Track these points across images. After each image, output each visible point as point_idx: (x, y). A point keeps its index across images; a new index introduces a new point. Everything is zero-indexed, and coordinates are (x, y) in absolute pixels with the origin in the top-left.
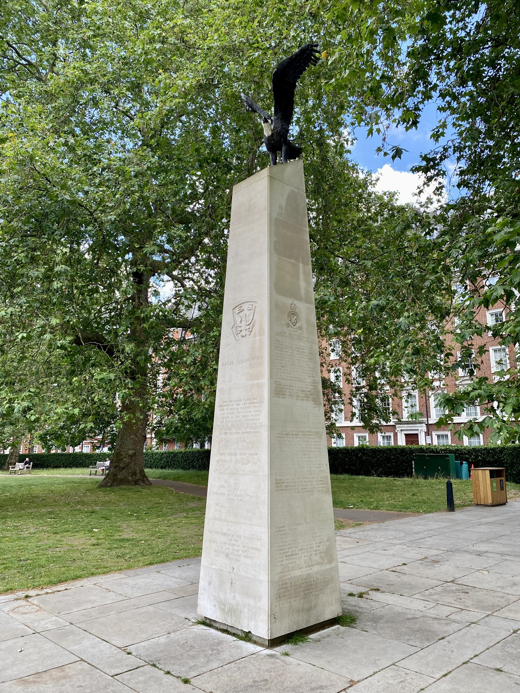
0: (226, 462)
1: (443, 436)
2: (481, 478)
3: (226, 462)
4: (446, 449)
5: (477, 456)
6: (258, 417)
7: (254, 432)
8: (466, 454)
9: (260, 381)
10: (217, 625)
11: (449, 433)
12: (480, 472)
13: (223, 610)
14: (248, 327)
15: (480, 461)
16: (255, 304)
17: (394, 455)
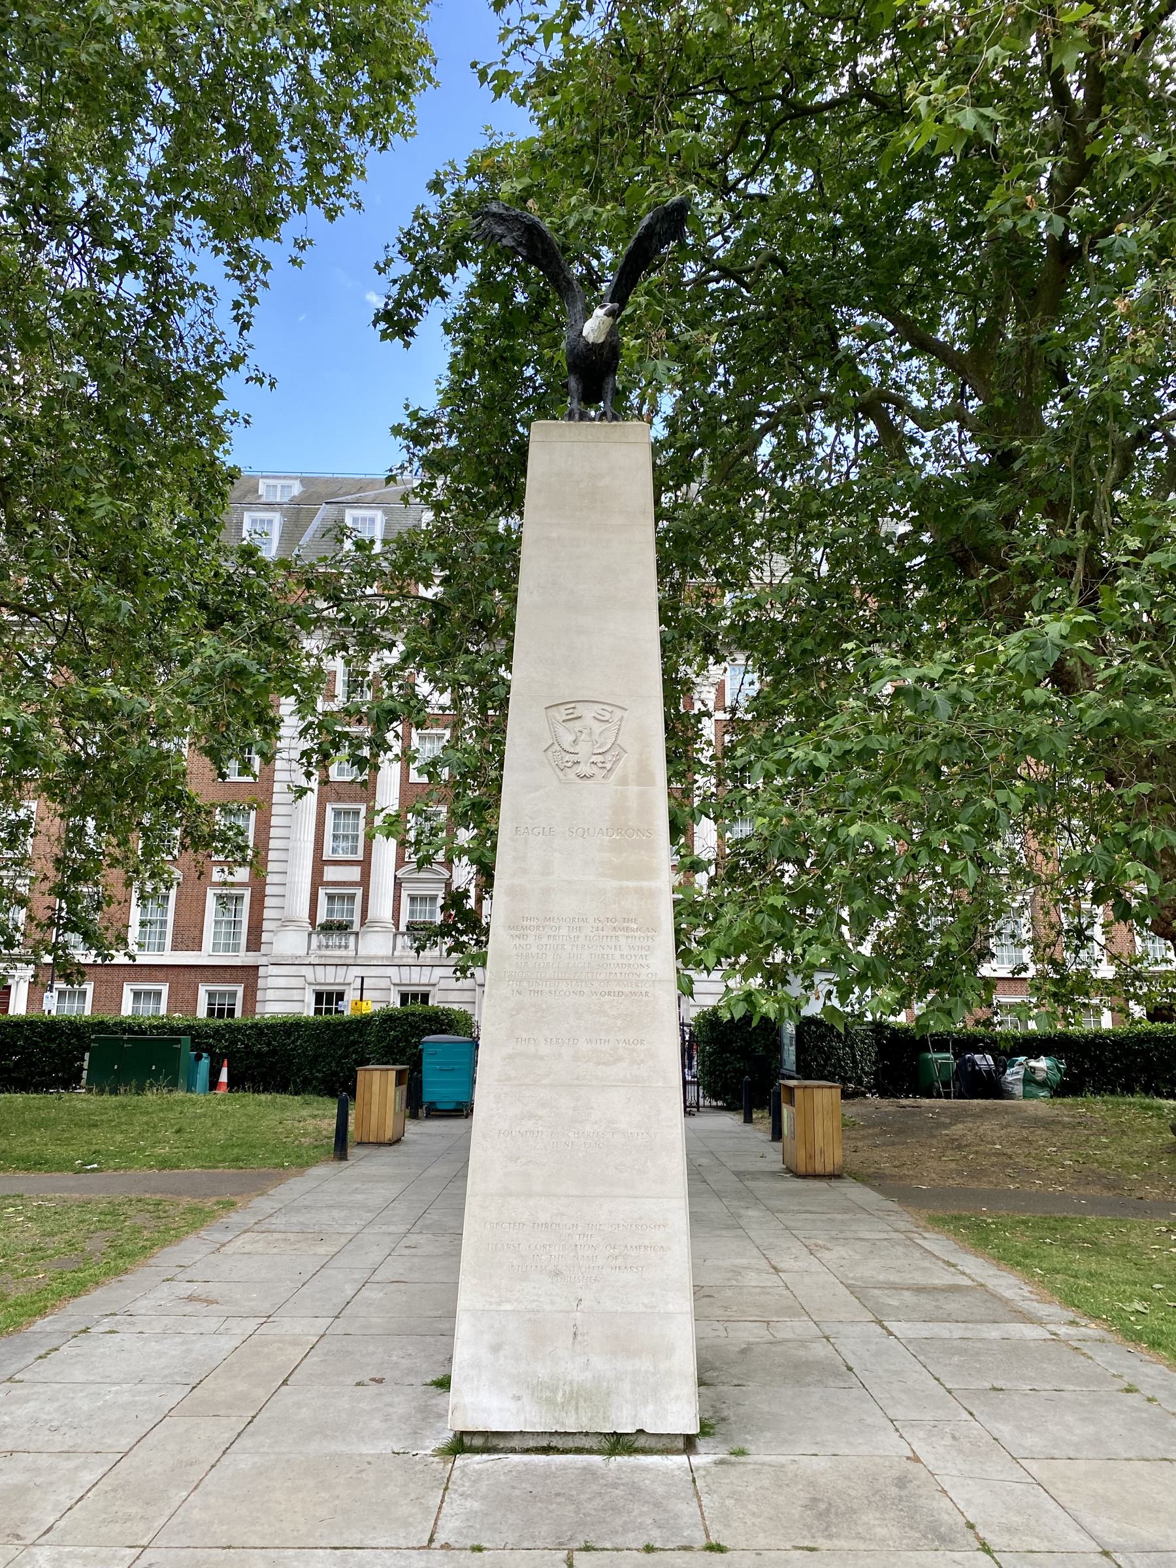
0: (542, 1058)
1: (148, 993)
2: (376, 1088)
3: (542, 1058)
5: (234, 1042)
6: (644, 962)
7: (633, 994)
9: (645, 884)
10: (515, 1443)
11: (165, 989)
12: (377, 1074)
13: (550, 1402)
14: (599, 758)
15: (238, 1051)
16: (619, 713)
17: (27, 1038)
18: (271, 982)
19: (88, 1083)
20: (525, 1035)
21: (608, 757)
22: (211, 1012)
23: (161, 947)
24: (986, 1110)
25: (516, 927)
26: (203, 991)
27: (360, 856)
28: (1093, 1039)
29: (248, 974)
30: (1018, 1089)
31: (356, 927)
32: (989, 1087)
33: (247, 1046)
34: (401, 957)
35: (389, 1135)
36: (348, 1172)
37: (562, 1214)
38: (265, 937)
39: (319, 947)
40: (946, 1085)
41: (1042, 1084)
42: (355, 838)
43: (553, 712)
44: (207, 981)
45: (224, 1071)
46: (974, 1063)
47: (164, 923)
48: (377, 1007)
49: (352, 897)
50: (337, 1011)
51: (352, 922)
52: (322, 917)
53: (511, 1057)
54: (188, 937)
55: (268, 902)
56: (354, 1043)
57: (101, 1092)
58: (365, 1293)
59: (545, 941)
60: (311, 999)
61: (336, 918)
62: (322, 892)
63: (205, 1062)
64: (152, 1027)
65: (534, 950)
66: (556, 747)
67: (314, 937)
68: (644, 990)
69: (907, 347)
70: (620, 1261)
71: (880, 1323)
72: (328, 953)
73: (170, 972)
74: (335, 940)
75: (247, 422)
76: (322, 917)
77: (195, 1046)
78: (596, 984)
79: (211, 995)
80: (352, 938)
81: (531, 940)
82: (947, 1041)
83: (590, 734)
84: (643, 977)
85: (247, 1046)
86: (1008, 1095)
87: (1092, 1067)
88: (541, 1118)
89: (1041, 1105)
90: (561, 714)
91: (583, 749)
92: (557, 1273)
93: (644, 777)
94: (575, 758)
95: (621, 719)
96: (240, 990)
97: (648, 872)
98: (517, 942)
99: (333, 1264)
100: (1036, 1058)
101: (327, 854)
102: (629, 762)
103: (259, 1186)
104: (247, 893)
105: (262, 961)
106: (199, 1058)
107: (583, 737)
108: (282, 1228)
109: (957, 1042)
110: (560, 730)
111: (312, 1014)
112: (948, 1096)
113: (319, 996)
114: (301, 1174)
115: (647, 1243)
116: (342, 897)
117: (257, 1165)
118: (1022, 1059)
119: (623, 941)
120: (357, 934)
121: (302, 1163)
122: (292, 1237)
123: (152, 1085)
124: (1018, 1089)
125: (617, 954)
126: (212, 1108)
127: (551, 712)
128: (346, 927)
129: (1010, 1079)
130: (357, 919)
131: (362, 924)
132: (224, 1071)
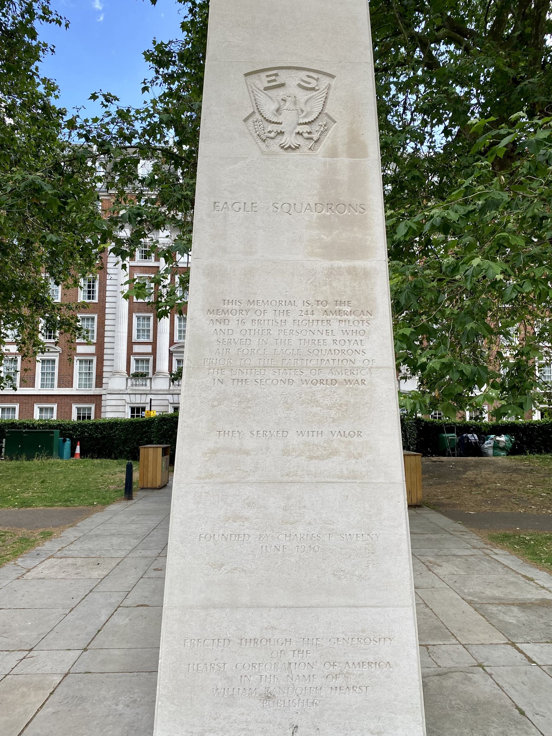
0: (247, 453)
1: (47, 409)
2: (151, 458)
3: (247, 453)
4: (46, 424)
5: (83, 432)
8: (69, 430)
9: (359, 263)
11: (55, 406)
14: (306, 128)
15: (86, 437)
16: (325, 81)
18: (108, 403)
19: (5, 454)
20: (227, 428)
21: (315, 127)
22: (79, 418)
23: (52, 386)
24: (476, 462)
25: (216, 312)
27: (151, 340)
28: (528, 426)
29: (97, 399)
30: (491, 452)
31: (150, 375)
32: (476, 450)
33: (90, 434)
34: (173, 390)
35: (159, 483)
36: (131, 508)
37: (273, 628)
38: (104, 381)
39: (132, 385)
40: (453, 450)
41: (503, 449)
42: (148, 331)
43: (253, 79)
44: (76, 402)
45: (78, 448)
46: (468, 439)
47: (53, 374)
48: (158, 414)
49: (148, 361)
50: (142, 417)
51: (148, 373)
52: (133, 370)
53: (214, 452)
54: (66, 380)
55: (105, 363)
56: (145, 432)
57: (11, 459)
58: (116, 619)
59: (248, 325)
60: (129, 411)
61: (140, 371)
62: (132, 358)
63: (68, 443)
64: (40, 425)
65: (237, 336)
66: (257, 116)
67: (129, 381)
68: (359, 377)
70: (340, 681)
71: (513, 644)
72: (137, 388)
73: (57, 398)
74: (140, 382)
75: (53, 51)
76: (133, 370)
77: (62, 435)
78: (306, 372)
79: (79, 409)
80: (148, 381)
81: (233, 325)
82: (454, 427)
83: (295, 103)
84: (358, 364)
85: (90, 434)
86: (486, 455)
87: (532, 440)
88: (247, 519)
89: (503, 460)
90: (262, 81)
91: (288, 119)
92: (268, 697)
93: (355, 148)
94: (278, 128)
95: (329, 87)
96: (93, 407)
98: (218, 326)
99: (101, 588)
100: (499, 435)
101: (135, 339)
102: (337, 134)
103: (71, 521)
104: (95, 359)
106: (64, 441)
108: (75, 554)
109: (458, 428)
110: (262, 98)
111: (130, 417)
112: (454, 455)
113: (133, 409)
114: (102, 510)
115: (371, 658)
116: (142, 360)
117: (82, 502)
118: (492, 436)
119: (335, 325)
120: (151, 379)
121: (105, 501)
122: (79, 561)
123: (38, 456)
124: (491, 452)
125: (329, 339)
126: (69, 468)
127: (251, 79)
128: (145, 375)
129: (486, 446)
130: (151, 371)
131: (154, 374)
132: (78, 448)
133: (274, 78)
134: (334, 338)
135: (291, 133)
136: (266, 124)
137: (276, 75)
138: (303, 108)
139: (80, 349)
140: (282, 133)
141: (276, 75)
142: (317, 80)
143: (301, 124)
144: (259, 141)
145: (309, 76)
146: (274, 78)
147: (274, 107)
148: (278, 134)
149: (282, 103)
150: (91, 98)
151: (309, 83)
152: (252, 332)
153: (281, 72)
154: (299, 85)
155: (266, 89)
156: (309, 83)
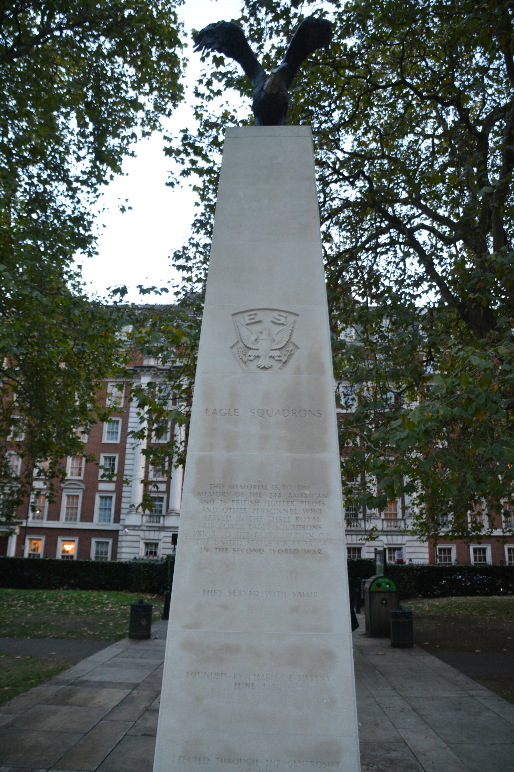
1: (102, 543)
14: (277, 353)
16: (291, 318)
26: (94, 541)
29: (114, 534)
38: (122, 517)
43: (239, 318)
60: (142, 546)
66: (241, 344)
69: (420, 211)
90: (246, 318)
94: (256, 353)
95: (295, 322)
97: (324, 447)
104: (114, 496)
105: (121, 528)
107: (263, 336)
110: (244, 331)
120: (164, 516)
133: (253, 317)
134: (296, 515)
135: (265, 357)
136: (247, 350)
137: (256, 314)
138: (275, 339)
139: (102, 486)
140: (259, 357)
141: (256, 314)
142: (286, 317)
143: (273, 350)
144: (241, 363)
145: (279, 315)
146: (253, 317)
147: (253, 338)
148: (256, 357)
149: (260, 334)
150: (123, 212)
151: (280, 320)
152: (232, 510)
153: (258, 312)
154: (273, 322)
155: (247, 325)
156: (280, 320)
